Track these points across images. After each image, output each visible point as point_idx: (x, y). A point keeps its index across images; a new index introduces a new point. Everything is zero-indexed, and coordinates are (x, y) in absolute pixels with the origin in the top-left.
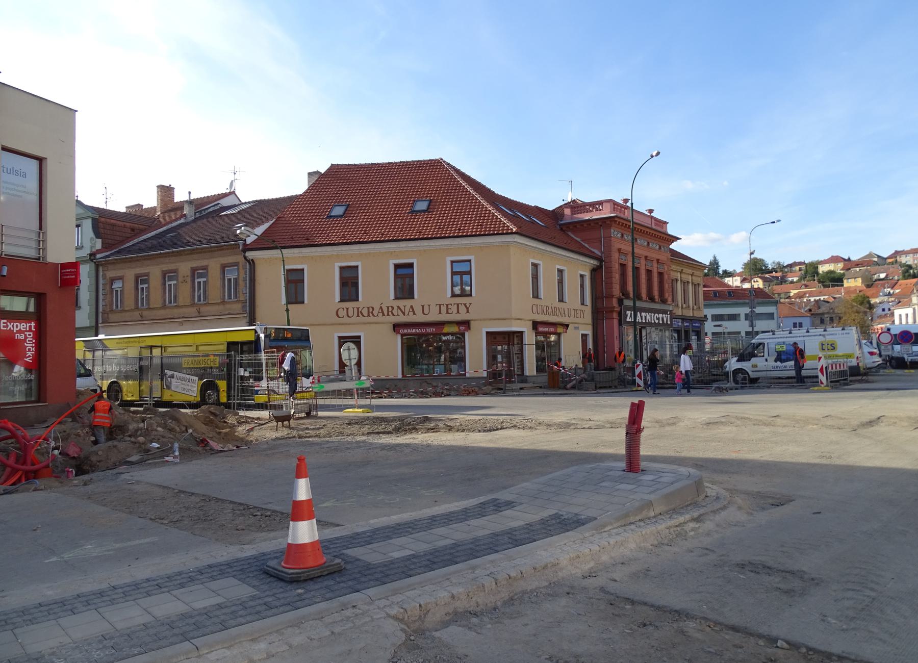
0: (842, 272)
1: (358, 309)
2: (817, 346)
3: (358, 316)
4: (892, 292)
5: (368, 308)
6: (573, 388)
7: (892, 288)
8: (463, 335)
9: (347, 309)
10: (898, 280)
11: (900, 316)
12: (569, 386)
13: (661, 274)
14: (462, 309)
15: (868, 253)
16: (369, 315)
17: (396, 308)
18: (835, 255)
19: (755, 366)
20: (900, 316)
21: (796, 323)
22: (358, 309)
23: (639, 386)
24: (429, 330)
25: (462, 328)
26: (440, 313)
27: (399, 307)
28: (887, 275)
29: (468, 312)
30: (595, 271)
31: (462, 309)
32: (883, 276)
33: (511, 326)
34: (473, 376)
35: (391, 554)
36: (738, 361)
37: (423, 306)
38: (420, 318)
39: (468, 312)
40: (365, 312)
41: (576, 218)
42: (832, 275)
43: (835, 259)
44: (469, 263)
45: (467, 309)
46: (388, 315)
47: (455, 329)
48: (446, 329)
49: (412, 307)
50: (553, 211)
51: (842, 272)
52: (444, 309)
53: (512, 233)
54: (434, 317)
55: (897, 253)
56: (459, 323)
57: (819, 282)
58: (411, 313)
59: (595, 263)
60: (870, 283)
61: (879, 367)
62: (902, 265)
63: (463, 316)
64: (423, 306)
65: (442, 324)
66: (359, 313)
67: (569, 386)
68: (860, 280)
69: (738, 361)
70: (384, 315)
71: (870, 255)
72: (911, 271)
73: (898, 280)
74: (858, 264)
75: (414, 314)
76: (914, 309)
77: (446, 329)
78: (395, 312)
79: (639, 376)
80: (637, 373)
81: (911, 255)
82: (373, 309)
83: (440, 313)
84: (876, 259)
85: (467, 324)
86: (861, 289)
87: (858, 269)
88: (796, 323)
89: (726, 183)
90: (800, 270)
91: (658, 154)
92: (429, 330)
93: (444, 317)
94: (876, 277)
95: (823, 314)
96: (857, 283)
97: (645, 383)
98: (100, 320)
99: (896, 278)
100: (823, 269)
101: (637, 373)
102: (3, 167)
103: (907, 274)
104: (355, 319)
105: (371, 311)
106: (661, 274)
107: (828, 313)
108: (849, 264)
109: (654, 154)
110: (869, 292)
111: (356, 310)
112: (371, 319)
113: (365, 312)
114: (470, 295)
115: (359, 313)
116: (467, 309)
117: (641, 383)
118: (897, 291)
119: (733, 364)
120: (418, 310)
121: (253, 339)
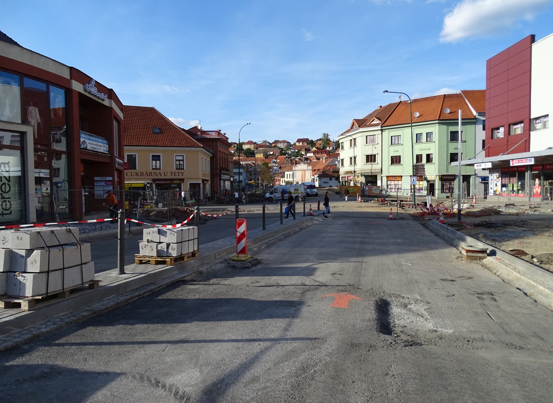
0: (254, 149)
1: (136, 173)
2: (294, 190)
3: (136, 175)
4: (276, 161)
5: (141, 173)
6: (226, 203)
7: (276, 159)
9: (131, 173)
10: (278, 156)
11: (287, 174)
12: (225, 203)
13: (227, 159)
14: (180, 174)
16: (150, 175)
17: (153, 173)
19: (275, 196)
20: (287, 174)
21: (421, 155)
22: (136, 173)
23: (244, 202)
24: (168, 182)
25: (181, 182)
26: (171, 175)
27: (154, 173)
28: (273, 153)
29: (182, 175)
30: (212, 158)
31: (180, 174)
32: (271, 153)
33: (199, 181)
36: (270, 194)
37: (164, 173)
38: (163, 177)
39: (182, 175)
40: (139, 174)
41: (203, 137)
42: (250, 151)
43: (250, 143)
44: (182, 157)
46: (150, 175)
47: (178, 182)
48: (175, 182)
49: (160, 173)
50: (188, 130)
51: (254, 149)
52: (173, 174)
53: (201, 147)
54: (169, 177)
55: (276, 142)
56: (180, 180)
57: (245, 154)
58: (160, 175)
59: (212, 155)
60: (267, 156)
61: (46, 196)
62: (279, 148)
63: (181, 177)
64: (164, 173)
65: (172, 180)
66: (137, 174)
67: (225, 203)
68: (262, 154)
69: (270, 194)
70: (148, 175)
71: (265, 142)
73: (278, 156)
74: (261, 146)
75: (161, 175)
76: (293, 172)
77: (175, 182)
78: (153, 174)
79: (244, 199)
80: (243, 198)
81: (282, 143)
82: (143, 173)
83: (171, 175)
84: (268, 144)
85: (183, 180)
86: (263, 159)
87: (261, 149)
88: (421, 155)
89: (189, 90)
90: (234, 147)
91: (250, 123)
92: (168, 182)
93: (173, 177)
94: (269, 153)
95: (251, 171)
96: (260, 156)
97: (246, 202)
98: (202, 186)
99: (277, 154)
100: (245, 147)
101: (243, 198)
104: (135, 177)
105: (142, 174)
106: (227, 159)
107: (253, 171)
108: (257, 146)
109: (249, 123)
110: (267, 161)
111: (135, 173)
112: (142, 177)
113: (139, 174)
114: (183, 169)
115: (137, 174)
116: (182, 174)
117: (245, 202)
118: (278, 161)
119: (268, 195)
120: (163, 174)
121: (143, 186)
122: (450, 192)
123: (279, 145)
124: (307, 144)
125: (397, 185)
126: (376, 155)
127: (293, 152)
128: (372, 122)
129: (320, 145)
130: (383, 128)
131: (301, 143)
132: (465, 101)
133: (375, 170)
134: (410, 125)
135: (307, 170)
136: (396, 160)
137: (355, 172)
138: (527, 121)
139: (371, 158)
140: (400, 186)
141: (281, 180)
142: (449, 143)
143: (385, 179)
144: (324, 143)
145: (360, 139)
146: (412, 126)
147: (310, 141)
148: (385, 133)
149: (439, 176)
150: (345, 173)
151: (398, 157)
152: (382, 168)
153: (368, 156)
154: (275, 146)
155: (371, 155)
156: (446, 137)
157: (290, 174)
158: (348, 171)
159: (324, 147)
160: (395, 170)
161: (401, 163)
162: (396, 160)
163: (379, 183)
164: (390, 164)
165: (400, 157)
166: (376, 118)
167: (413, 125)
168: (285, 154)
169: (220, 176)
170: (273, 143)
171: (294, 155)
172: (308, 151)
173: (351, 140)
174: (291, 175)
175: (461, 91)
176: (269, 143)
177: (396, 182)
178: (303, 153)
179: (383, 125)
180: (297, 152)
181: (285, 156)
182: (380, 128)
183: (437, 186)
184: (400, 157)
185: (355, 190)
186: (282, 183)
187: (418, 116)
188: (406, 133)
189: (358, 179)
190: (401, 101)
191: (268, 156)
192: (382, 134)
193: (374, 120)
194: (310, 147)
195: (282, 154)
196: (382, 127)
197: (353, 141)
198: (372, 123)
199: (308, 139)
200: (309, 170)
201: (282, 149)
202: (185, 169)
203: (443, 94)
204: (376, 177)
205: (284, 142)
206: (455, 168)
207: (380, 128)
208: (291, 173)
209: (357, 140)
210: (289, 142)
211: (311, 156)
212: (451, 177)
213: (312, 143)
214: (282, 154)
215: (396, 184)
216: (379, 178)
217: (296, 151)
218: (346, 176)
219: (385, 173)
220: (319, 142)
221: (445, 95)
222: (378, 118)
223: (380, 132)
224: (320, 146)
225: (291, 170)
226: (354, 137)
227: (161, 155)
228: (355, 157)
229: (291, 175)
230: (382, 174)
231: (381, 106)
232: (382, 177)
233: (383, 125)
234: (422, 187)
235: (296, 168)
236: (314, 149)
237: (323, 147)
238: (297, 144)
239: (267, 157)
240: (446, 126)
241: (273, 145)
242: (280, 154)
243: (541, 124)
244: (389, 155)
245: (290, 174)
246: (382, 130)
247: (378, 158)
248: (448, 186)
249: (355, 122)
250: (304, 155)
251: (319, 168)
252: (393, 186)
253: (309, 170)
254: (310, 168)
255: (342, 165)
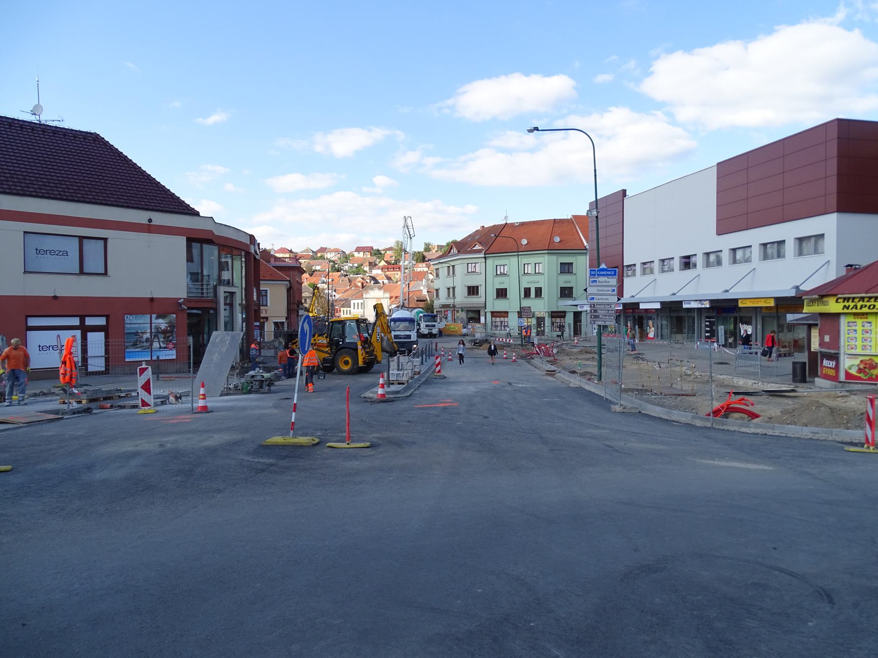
8: (264, 323)
11: (354, 304)
15: (306, 248)
18: (283, 247)
20: (354, 304)
21: (529, 289)
25: (265, 320)
29: (266, 313)
34: (268, 341)
35: (268, 440)
39: (266, 313)
44: (26, 271)
45: (266, 312)
55: (323, 250)
72: (336, 266)
84: (311, 254)
88: (529, 289)
94: (314, 268)
102: (37, 249)
103: (334, 268)
114: (267, 306)
116: (266, 312)
122: (560, 331)
123: (329, 256)
124: (371, 255)
125: (503, 323)
126: (479, 287)
127: (351, 267)
128: (474, 247)
129: (391, 257)
130: (487, 256)
131: (362, 253)
132: (576, 228)
133: (478, 304)
134: (517, 254)
135: (383, 298)
136: (502, 293)
137: (454, 306)
138: (621, 267)
139: (473, 291)
140: (506, 324)
141: (342, 312)
142: (559, 276)
143: (489, 315)
144: (396, 255)
145: (460, 269)
146: (518, 255)
147: (375, 250)
148: (489, 261)
149: (548, 312)
150: (441, 306)
151: (504, 290)
152: (486, 302)
153: (469, 288)
154: (322, 258)
155: (473, 287)
156: (557, 268)
157: (358, 303)
158: (445, 305)
159: (397, 261)
160: (501, 305)
161: (508, 297)
162: (502, 293)
163: (482, 319)
164: (495, 297)
165: (506, 289)
166: (479, 242)
167: (519, 253)
168: (338, 271)
169: (298, 312)
170: (319, 251)
171: (353, 271)
172: (372, 265)
173: (449, 267)
174: (360, 304)
175: (573, 216)
176: (313, 252)
177: (502, 319)
178: (367, 269)
179: (486, 252)
180: (357, 267)
181: (339, 273)
182: (483, 256)
183: (548, 322)
184: (506, 289)
185: (456, 328)
186: (344, 314)
187: (526, 243)
188: (510, 264)
189: (458, 314)
190: (506, 223)
191: (314, 272)
192: (486, 262)
193: (476, 245)
194: (376, 260)
195: (335, 269)
196: (485, 254)
197: (451, 267)
198: (474, 248)
199: (372, 248)
200: (386, 298)
201: (333, 262)
202: (268, 305)
203: (553, 218)
204: (479, 312)
205: (336, 251)
206: (565, 304)
207: (483, 256)
208: (360, 301)
209: (456, 267)
210: (343, 252)
211: (377, 274)
212: (561, 314)
213: (378, 253)
214: (335, 269)
215: (502, 322)
216: (482, 313)
217: (356, 265)
218: (443, 310)
219: (489, 309)
220: (388, 252)
221: (555, 220)
222: (480, 243)
223: (484, 260)
224: (390, 259)
225: (361, 297)
226: (452, 263)
227: (268, 289)
228: (454, 288)
229: (360, 304)
230: (486, 309)
231: (483, 227)
232: (486, 312)
233: (486, 252)
234: (531, 325)
235: (368, 296)
236: (383, 263)
237: (395, 261)
238: (356, 254)
239: (312, 274)
240: (556, 257)
241: (319, 255)
242: (332, 269)
243: (631, 271)
244: (493, 287)
245: (358, 303)
246: (485, 258)
247: (481, 291)
248: (559, 324)
249: (453, 246)
250: (367, 272)
251: (397, 295)
252: (499, 323)
253: (386, 298)
254: (388, 295)
255: (437, 296)
